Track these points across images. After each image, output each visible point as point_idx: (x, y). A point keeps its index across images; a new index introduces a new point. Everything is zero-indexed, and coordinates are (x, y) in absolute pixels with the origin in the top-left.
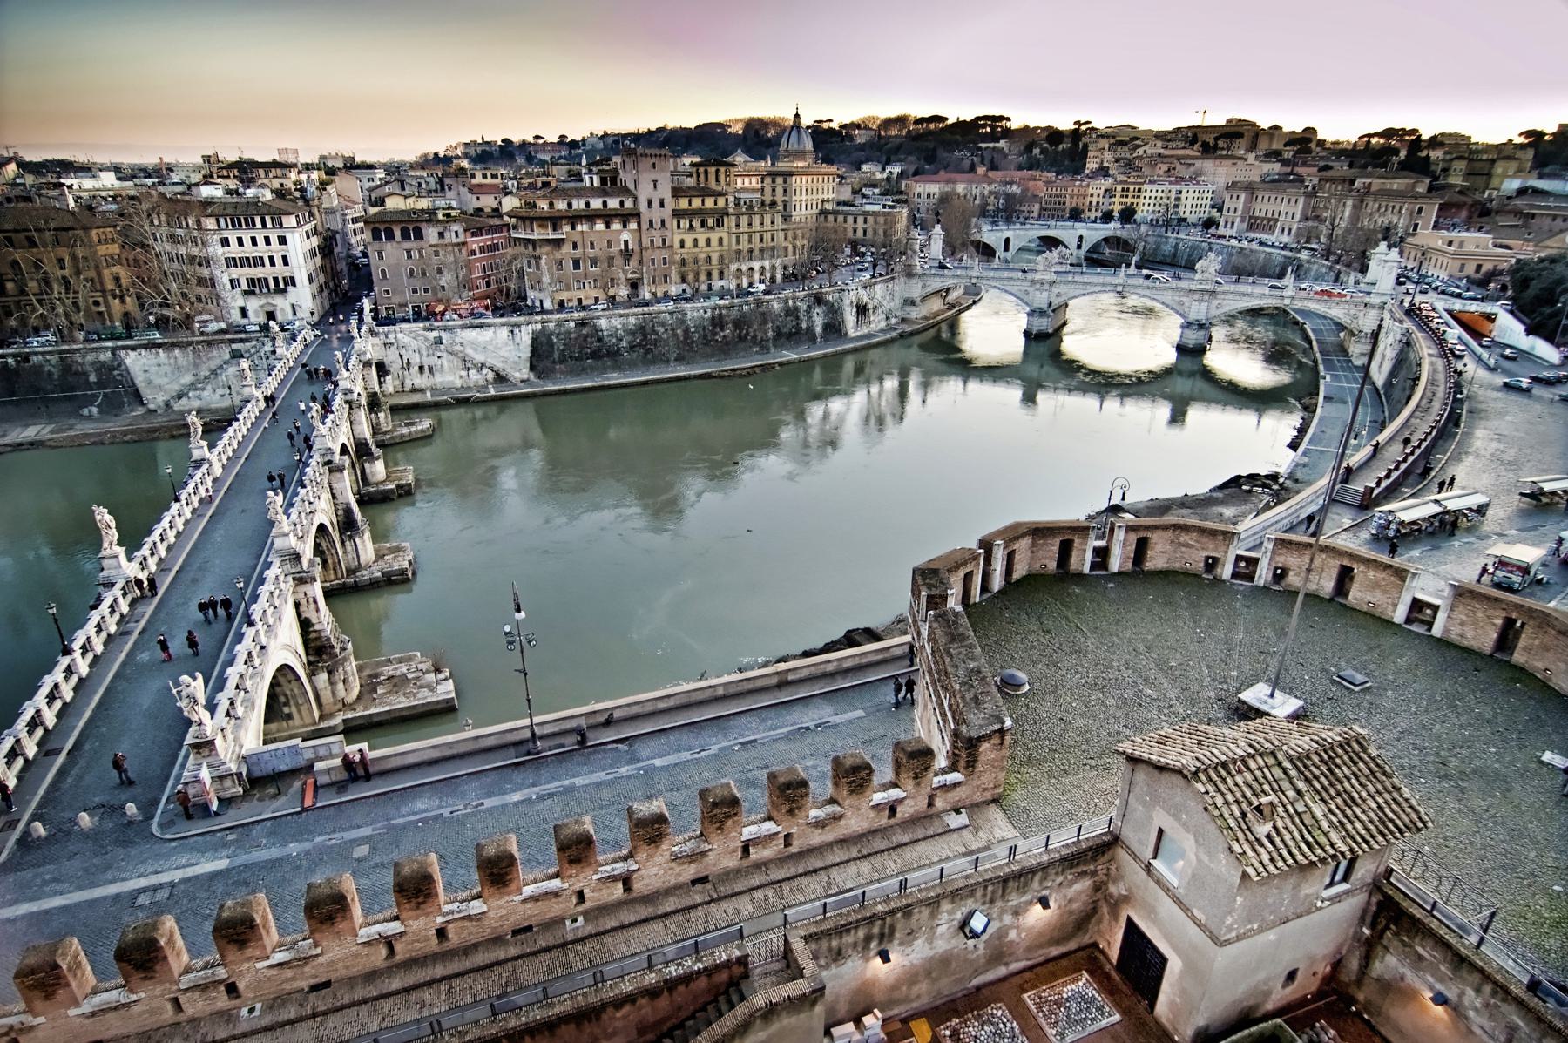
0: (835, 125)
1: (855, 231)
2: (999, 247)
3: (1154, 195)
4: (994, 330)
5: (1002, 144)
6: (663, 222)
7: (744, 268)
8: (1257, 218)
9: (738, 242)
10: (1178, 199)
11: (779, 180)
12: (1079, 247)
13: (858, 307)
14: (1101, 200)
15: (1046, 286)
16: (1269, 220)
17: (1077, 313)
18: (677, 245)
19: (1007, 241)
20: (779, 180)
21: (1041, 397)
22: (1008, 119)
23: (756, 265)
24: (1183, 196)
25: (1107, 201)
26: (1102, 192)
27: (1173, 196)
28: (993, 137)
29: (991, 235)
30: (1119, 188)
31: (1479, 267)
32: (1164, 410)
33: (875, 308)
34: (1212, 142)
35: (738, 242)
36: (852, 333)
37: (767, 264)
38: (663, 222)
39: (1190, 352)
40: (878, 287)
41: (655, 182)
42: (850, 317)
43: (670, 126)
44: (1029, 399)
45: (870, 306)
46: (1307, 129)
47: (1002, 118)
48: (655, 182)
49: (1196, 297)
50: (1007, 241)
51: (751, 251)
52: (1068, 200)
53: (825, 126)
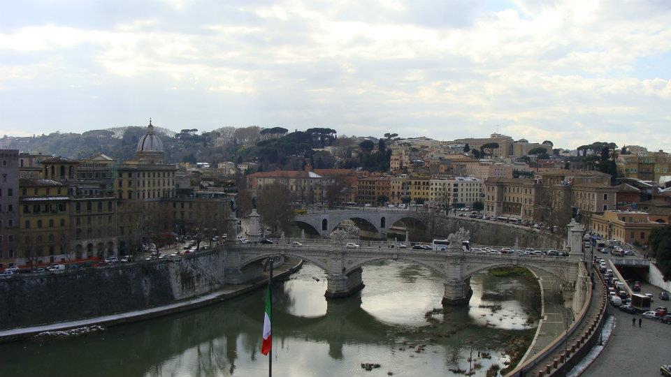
0: (199, 133)
1: (182, 213)
2: (378, 225)
3: (438, 187)
4: (309, 294)
5: (328, 149)
6: (10, 207)
7: (85, 243)
8: (508, 204)
9: (78, 223)
10: (456, 190)
11: (125, 175)
12: (383, 225)
13: (182, 275)
14: (401, 191)
15: (340, 256)
16: (517, 204)
17: (369, 275)
18: (23, 225)
19: (325, 222)
20: (125, 175)
21: (347, 349)
22: (334, 132)
23: (95, 242)
24: (460, 188)
25: (405, 191)
26: (401, 184)
27: (452, 188)
28: (323, 144)
29: (313, 216)
30: (413, 182)
31: (643, 235)
32: (324, 347)
33: (199, 276)
34: (479, 150)
35: (78, 223)
36: (177, 296)
37: (95, 242)
38: (10, 207)
39: (456, 305)
40: (201, 259)
41: (5, 176)
42: (176, 284)
43: (62, 132)
44: (336, 353)
45: (195, 274)
46: (545, 142)
47: (329, 131)
48: (5, 176)
50: (325, 222)
51: (90, 231)
53: (192, 133)
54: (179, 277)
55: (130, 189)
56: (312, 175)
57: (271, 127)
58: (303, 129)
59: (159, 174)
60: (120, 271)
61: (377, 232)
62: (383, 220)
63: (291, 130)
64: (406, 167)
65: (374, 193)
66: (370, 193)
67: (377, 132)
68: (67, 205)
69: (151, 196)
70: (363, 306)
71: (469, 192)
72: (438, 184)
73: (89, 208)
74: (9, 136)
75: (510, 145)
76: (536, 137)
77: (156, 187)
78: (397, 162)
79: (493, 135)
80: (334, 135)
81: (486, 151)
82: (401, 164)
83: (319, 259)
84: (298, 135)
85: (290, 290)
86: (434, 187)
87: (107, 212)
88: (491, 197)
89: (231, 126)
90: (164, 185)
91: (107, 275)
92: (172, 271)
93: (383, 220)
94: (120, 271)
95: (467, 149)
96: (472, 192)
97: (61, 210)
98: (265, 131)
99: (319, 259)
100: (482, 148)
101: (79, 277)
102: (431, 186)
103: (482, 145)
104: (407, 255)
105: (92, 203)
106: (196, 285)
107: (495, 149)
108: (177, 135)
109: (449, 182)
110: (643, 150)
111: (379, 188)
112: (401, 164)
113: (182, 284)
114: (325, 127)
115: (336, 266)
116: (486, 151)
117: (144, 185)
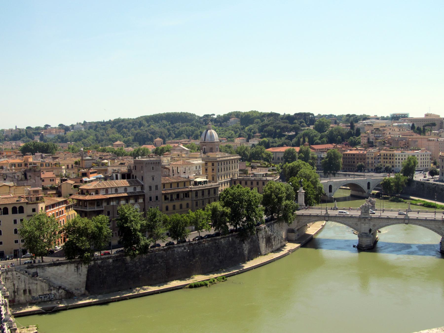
2: (365, 187)
49: (363, 221)
54: (264, 240)
55: (213, 173)
56: (82, 149)
60: (230, 239)
61: (365, 192)
62: (369, 184)
64: (372, 142)
65: (354, 162)
67: (306, 111)
68: (190, 193)
70: (441, 237)
71: (422, 161)
73: (203, 194)
74: (87, 121)
75: (326, 115)
76: (346, 114)
78: (365, 138)
79: (426, 115)
82: (368, 139)
84: (289, 118)
87: (207, 197)
89: (437, 113)
91: (223, 242)
92: (260, 236)
93: (369, 184)
94: (230, 239)
95: (413, 127)
96: (424, 161)
97: (186, 197)
100: (424, 126)
102: (396, 157)
105: (210, 190)
106: (273, 243)
109: (409, 153)
112: (368, 139)
115: (365, 227)
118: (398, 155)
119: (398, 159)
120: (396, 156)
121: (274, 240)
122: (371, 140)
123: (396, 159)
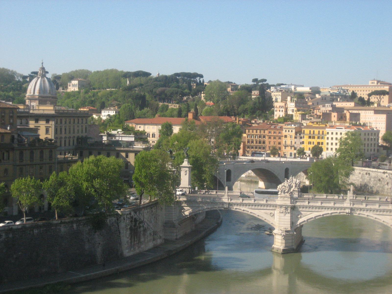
3: (334, 136)
22: (201, 76)
47: (196, 75)
52: (267, 139)
54: (128, 232)
57: (133, 69)
58: (169, 72)
59: (61, 120)
60: (75, 226)
63: (154, 75)
65: (264, 142)
66: (260, 142)
69: (67, 144)
70: (302, 261)
72: (334, 133)
77: (72, 135)
78: (281, 109)
80: (201, 79)
81: (373, 99)
83: (266, 213)
85: (206, 244)
86: (330, 136)
88: (370, 145)
90: (65, 133)
94: (75, 226)
98: (127, 75)
99: (266, 213)
100: (370, 95)
101: (36, 231)
102: (328, 136)
103: (370, 92)
104: (237, 205)
106: (142, 240)
107: (382, 96)
108: (256, 225)
110: (116, 71)
111: (274, 138)
113: (131, 239)
114: (192, 71)
116: (373, 99)
117: (61, 133)
118: (330, 133)
119: (330, 139)
120: (328, 133)
121: (144, 235)
122: (290, 112)
123: (328, 138)
